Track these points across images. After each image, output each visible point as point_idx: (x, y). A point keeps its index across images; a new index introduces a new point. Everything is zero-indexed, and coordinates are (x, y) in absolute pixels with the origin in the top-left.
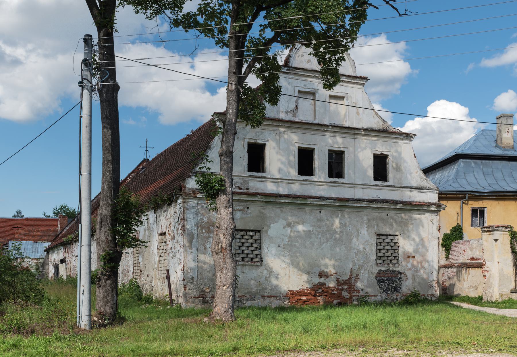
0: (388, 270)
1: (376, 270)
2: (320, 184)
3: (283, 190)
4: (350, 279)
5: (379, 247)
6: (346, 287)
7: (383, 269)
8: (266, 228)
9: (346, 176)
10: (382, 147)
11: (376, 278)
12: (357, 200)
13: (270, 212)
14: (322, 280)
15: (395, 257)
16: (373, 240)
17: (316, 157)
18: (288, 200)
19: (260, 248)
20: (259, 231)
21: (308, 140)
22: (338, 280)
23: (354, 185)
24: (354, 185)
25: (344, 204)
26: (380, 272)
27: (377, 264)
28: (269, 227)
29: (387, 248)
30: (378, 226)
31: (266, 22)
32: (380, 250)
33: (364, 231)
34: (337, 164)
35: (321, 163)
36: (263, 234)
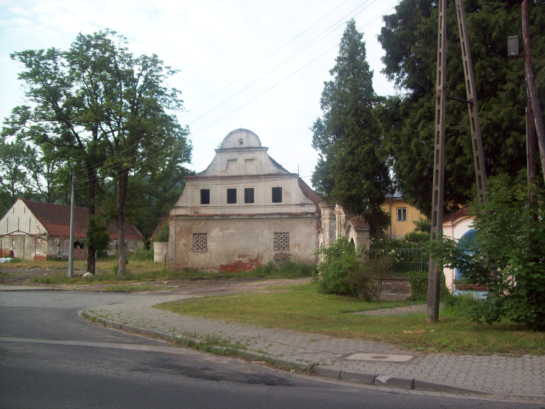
0: (282, 253)
1: (273, 253)
2: (240, 207)
3: (219, 212)
4: (257, 259)
5: (276, 240)
6: (255, 263)
7: (278, 253)
8: (209, 232)
9: (255, 201)
10: (277, 183)
11: (274, 258)
12: (260, 214)
13: (211, 223)
14: (240, 259)
15: (286, 246)
16: (272, 236)
17: (283, 191)
18: (277, 216)
19: (206, 243)
20: (206, 234)
21: (232, 185)
22: (250, 259)
23: (215, 207)
24: (215, 207)
25: (251, 217)
26: (276, 255)
27: (274, 250)
28: (211, 232)
29: (281, 240)
30: (275, 228)
31: (32, 173)
32: (276, 242)
33: (266, 231)
34: (249, 196)
35: (240, 195)
36: (208, 236)
